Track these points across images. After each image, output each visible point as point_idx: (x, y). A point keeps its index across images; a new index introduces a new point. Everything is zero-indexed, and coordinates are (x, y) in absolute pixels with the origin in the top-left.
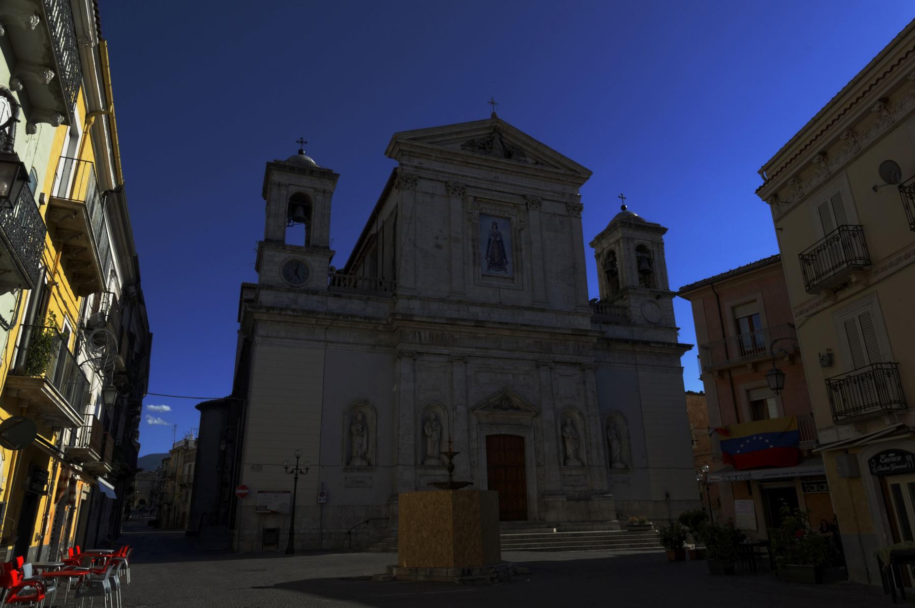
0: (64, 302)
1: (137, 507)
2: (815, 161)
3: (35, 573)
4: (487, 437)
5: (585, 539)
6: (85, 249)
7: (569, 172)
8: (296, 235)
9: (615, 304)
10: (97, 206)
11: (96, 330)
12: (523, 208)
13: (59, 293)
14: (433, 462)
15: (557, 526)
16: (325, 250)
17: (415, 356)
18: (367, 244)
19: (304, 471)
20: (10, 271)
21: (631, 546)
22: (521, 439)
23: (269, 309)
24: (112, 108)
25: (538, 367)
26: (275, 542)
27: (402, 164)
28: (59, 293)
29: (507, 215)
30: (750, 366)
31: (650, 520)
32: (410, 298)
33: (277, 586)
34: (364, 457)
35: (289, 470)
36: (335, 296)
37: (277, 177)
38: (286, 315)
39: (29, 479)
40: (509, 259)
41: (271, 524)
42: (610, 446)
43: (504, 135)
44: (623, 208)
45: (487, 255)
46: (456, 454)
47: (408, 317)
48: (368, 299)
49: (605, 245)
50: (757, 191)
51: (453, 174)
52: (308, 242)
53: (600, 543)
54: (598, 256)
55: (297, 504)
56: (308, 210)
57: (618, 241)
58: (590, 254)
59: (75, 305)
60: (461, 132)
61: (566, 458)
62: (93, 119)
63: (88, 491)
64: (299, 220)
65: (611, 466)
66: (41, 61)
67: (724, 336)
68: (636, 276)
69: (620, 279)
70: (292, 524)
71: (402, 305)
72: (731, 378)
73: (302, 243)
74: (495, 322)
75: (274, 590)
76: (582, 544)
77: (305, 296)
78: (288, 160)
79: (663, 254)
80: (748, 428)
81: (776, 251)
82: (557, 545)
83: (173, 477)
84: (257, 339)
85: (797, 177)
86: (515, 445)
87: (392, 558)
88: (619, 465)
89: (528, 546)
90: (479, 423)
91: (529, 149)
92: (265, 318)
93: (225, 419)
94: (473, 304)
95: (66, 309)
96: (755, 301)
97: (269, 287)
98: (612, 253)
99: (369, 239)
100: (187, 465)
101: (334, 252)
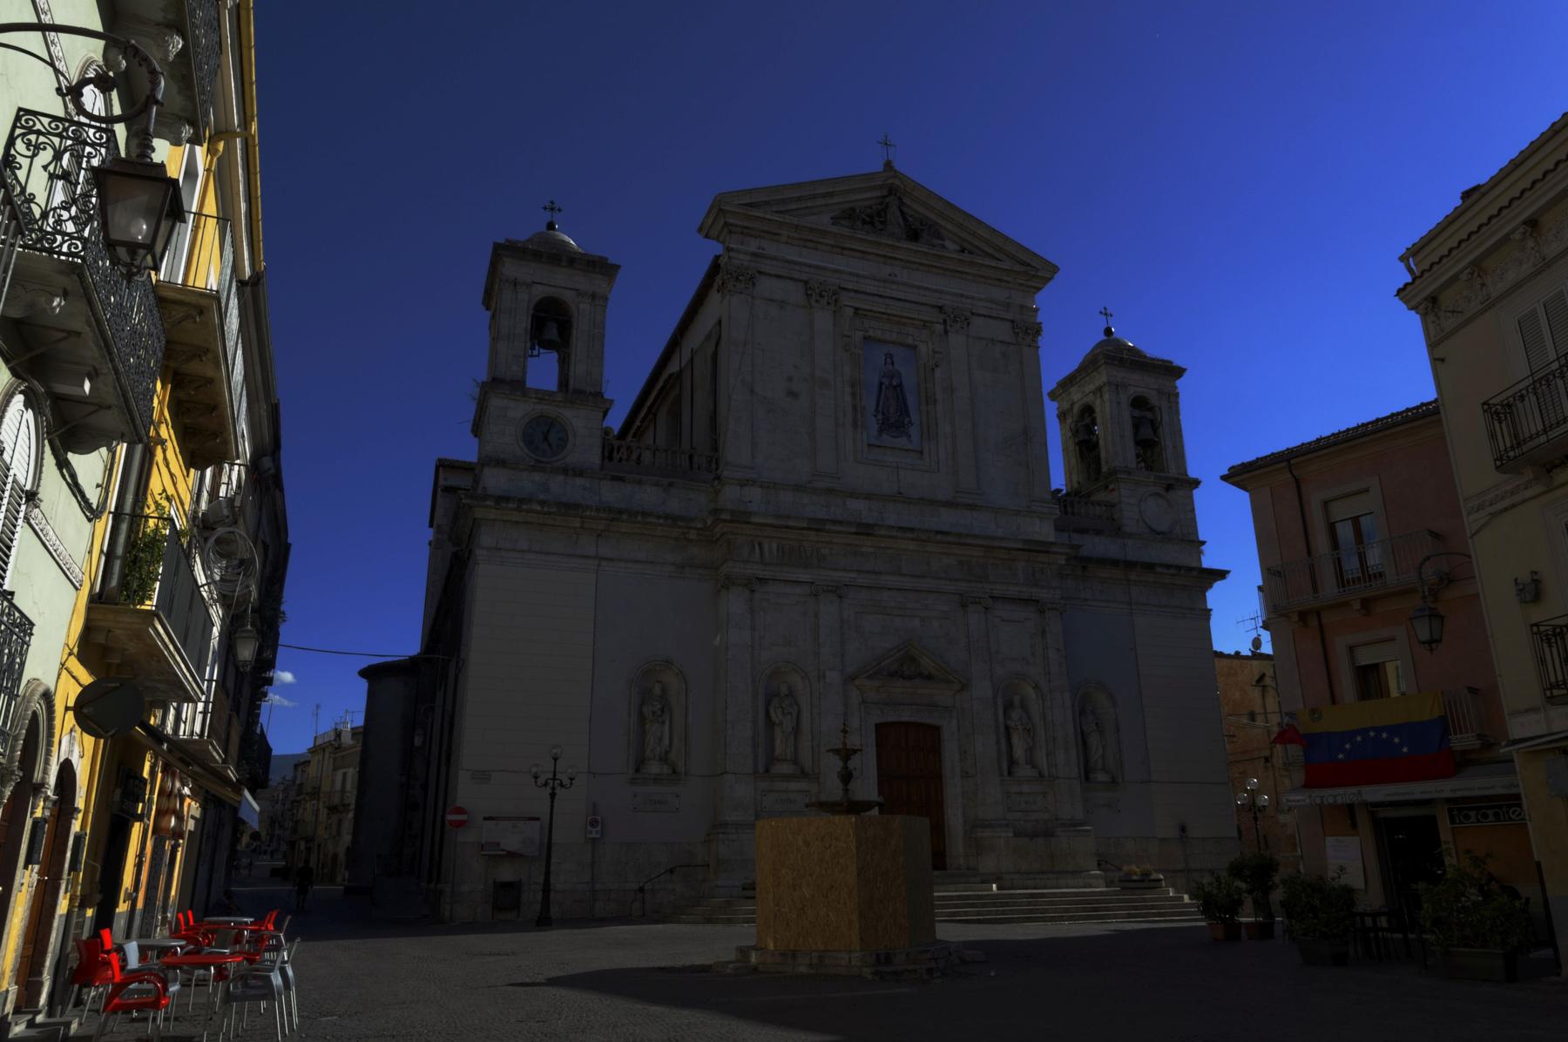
0: (172, 475)
1: (248, 846)
2: (1517, 236)
3: (143, 956)
4: (877, 726)
5: (1051, 903)
6: (210, 381)
7: (1018, 268)
8: (543, 371)
9: (1094, 498)
10: (234, 302)
11: (221, 531)
12: (939, 328)
13: (165, 459)
14: (786, 768)
15: (998, 879)
16: (597, 399)
17: (753, 584)
18: (662, 389)
19: (566, 782)
20: (109, 407)
21: (1129, 916)
22: (936, 729)
23: (501, 499)
24: (254, 127)
25: (964, 606)
26: (509, 906)
27: (729, 250)
28: (165, 459)
29: (910, 341)
30: (1357, 605)
31: (1158, 871)
32: (743, 483)
33: (553, 982)
34: (664, 759)
35: (541, 781)
36: (614, 478)
37: (510, 269)
38: (528, 511)
39: (118, 792)
40: (914, 417)
41: (506, 873)
42: (1085, 743)
43: (906, 201)
44: (1108, 332)
45: (877, 410)
46: (855, 751)
47: (741, 517)
48: (671, 485)
49: (1077, 396)
50: (1399, 291)
51: (818, 267)
52: (564, 383)
53: (1077, 910)
54: (1062, 416)
55: (555, 838)
56: (565, 327)
57: (1100, 389)
58: (1051, 409)
59: (186, 483)
60: (831, 194)
61: (1012, 762)
62: (221, 146)
63: (198, 815)
64: (548, 345)
65: (1087, 779)
66: (159, 16)
67: (1309, 553)
68: (1131, 451)
69: (1103, 455)
70: (548, 873)
71: (730, 495)
72: (1321, 626)
73: (552, 385)
74: (890, 527)
75: (552, 991)
76: (1046, 911)
77: (561, 478)
78: (530, 240)
79: (1177, 412)
80: (1349, 714)
81: (1430, 394)
82: (1003, 913)
83: (315, 793)
84: (479, 553)
85: (1477, 267)
86: (929, 738)
87: (745, 934)
88: (1101, 777)
89: (954, 914)
90: (863, 702)
91: (949, 226)
92: (492, 516)
93: (417, 696)
94: (853, 495)
95: (175, 487)
96: (1367, 490)
97: (501, 463)
98: (1088, 410)
99: (667, 381)
100: (340, 774)
101: (611, 401)
